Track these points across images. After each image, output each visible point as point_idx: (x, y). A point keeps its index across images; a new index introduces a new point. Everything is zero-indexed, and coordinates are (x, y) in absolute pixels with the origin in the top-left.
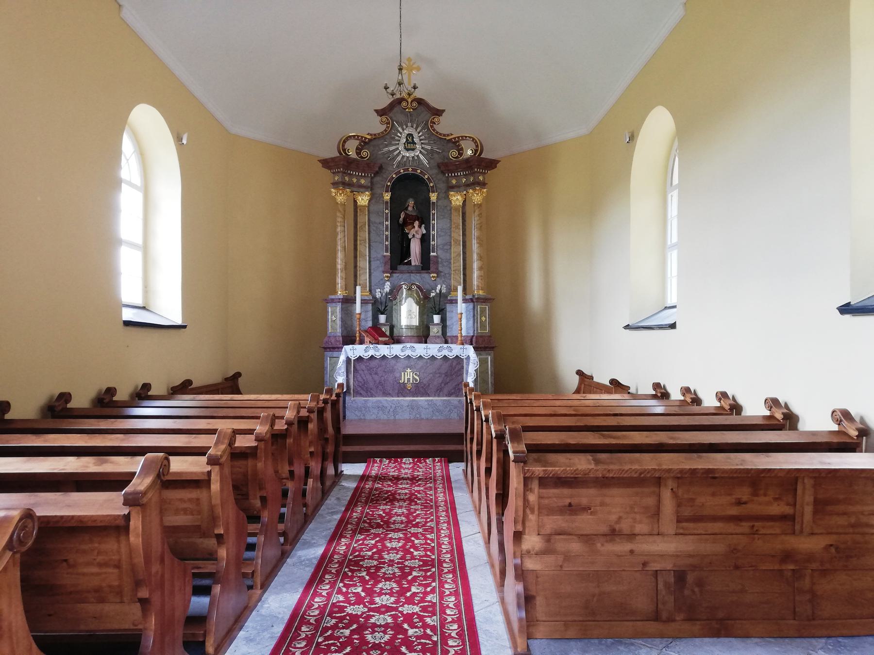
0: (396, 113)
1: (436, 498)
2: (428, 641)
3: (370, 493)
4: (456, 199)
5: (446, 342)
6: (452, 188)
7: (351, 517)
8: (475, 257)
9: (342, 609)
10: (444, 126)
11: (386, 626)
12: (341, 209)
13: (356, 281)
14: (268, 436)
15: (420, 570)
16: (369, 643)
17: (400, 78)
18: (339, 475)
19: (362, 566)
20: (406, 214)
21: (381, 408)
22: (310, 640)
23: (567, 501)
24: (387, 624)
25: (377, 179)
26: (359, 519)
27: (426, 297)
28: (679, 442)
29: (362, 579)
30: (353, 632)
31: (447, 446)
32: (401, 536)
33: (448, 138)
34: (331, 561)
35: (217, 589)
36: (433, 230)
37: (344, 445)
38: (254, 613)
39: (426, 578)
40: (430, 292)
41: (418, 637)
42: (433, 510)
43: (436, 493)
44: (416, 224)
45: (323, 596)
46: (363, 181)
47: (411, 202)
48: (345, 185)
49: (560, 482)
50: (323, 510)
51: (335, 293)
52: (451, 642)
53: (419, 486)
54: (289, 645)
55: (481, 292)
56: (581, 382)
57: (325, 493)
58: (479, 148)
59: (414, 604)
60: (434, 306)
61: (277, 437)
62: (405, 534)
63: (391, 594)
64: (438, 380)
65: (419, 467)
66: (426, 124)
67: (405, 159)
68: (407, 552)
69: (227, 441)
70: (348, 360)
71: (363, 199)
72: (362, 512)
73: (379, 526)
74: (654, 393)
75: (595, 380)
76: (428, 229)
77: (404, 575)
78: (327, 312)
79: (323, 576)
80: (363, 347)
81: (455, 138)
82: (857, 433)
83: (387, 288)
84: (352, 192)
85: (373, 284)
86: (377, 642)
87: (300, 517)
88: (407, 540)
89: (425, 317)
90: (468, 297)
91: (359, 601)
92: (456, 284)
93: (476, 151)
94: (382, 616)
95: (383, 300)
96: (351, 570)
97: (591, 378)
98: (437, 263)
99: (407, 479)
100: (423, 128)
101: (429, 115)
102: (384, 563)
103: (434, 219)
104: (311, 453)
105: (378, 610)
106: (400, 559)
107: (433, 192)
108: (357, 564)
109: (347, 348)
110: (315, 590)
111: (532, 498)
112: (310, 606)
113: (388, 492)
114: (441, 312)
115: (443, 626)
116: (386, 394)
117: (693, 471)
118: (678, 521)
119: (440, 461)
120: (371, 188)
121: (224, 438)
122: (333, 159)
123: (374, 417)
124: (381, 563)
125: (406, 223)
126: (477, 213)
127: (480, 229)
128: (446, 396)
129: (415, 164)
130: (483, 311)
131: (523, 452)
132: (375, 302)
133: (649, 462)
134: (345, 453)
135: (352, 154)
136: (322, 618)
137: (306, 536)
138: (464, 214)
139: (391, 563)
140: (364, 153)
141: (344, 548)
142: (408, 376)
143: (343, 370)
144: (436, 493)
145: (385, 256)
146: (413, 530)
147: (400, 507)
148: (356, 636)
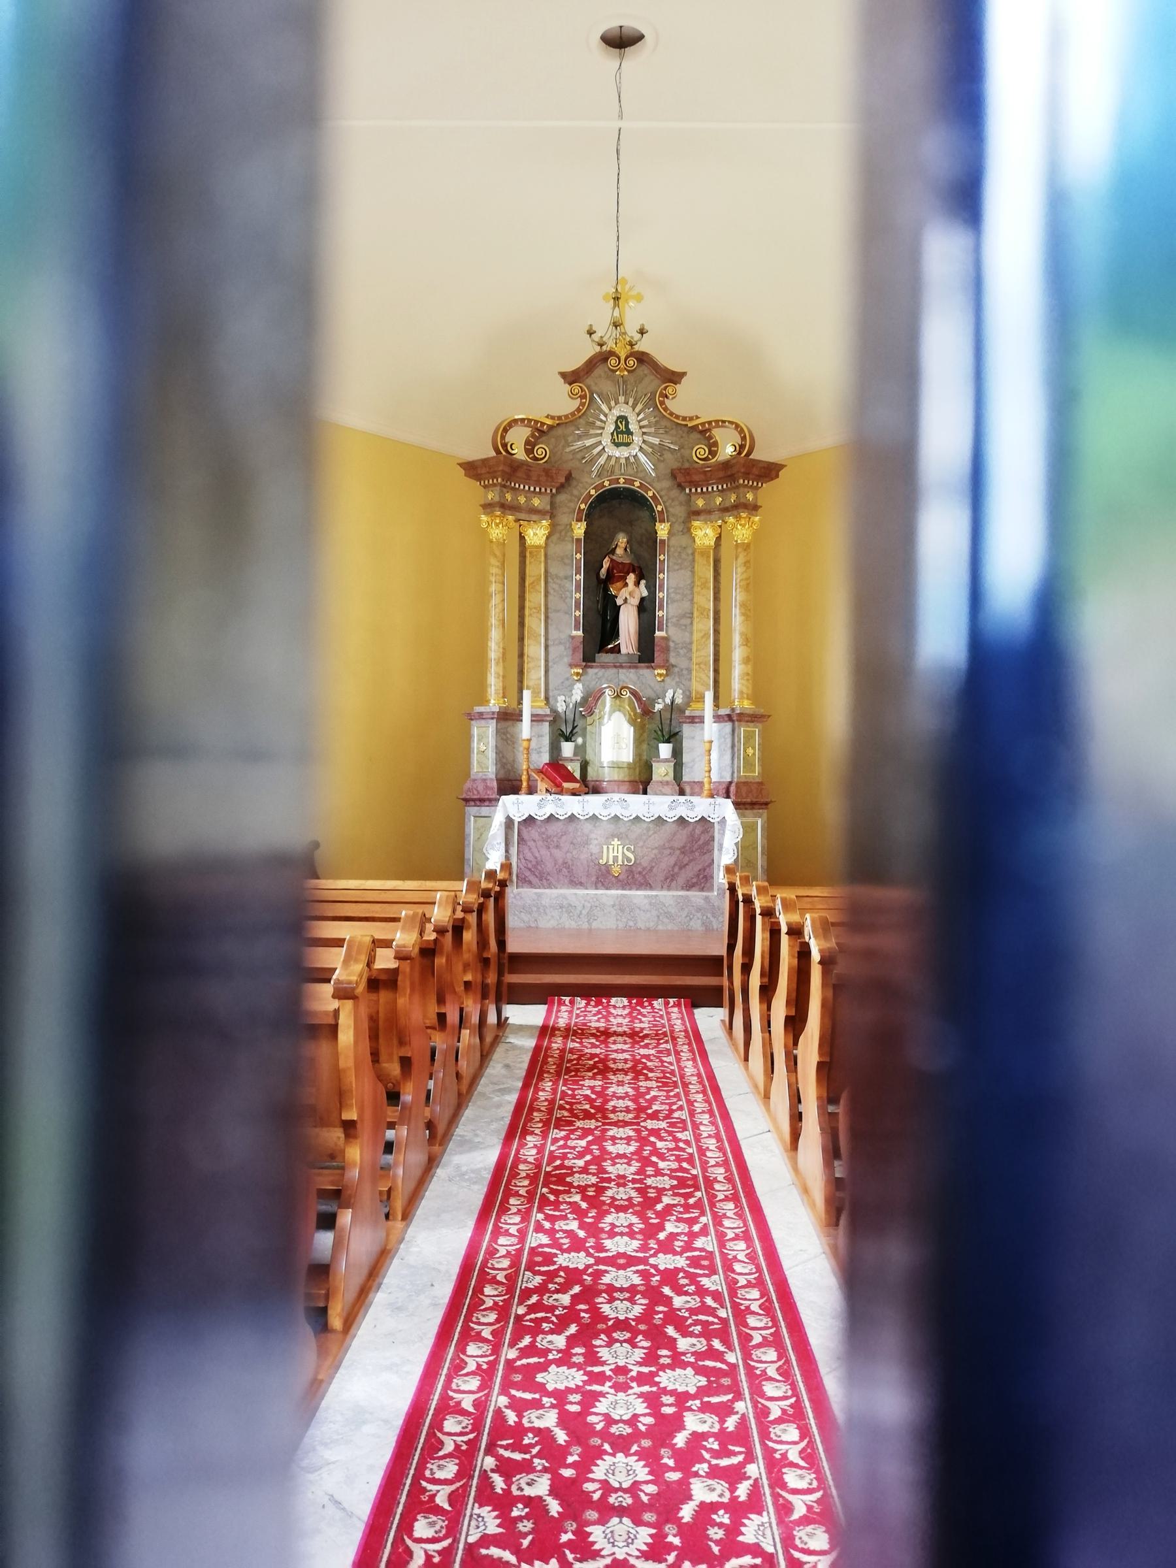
0: (600, 381)
1: (681, 1069)
2: (711, 1319)
3: (562, 1057)
4: (704, 534)
5: (682, 793)
6: (697, 513)
7: (535, 1099)
8: (737, 639)
9: (549, 1259)
10: (685, 402)
11: (632, 1290)
12: (498, 553)
13: (521, 681)
14: (417, 950)
15: (675, 1195)
16: (606, 1319)
17: (616, 313)
18: (502, 1023)
19: (570, 1185)
20: (612, 560)
21: (565, 908)
22: (503, 1311)
24: (633, 1286)
25: (562, 498)
26: (552, 1102)
27: (647, 711)
29: (575, 1207)
30: (576, 1299)
31: (693, 980)
32: (632, 1133)
33: (690, 424)
34: (514, 1174)
35: (345, 1218)
36: (661, 590)
37: (513, 973)
38: (396, 1262)
39: (687, 1208)
40: (653, 701)
41: (693, 1312)
42: (680, 1090)
43: (678, 1060)
44: (631, 578)
45: (485, 1340)
46: (536, 502)
47: (622, 540)
48: (505, 507)
50: (483, 1085)
51: (484, 701)
52: (752, 1321)
53: (646, 1046)
54: (468, 1318)
57: (485, 1056)
58: (746, 444)
59: (675, 1253)
60: (661, 727)
61: (428, 952)
62: (638, 1131)
63: (631, 1235)
64: (668, 862)
65: (640, 1013)
66: (652, 398)
67: (613, 462)
68: (646, 1162)
69: (364, 958)
70: (509, 823)
71: (537, 534)
72: (554, 1091)
73: (587, 1116)
76: (651, 588)
77: (649, 1203)
78: (469, 737)
79: (505, 1200)
80: (535, 798)
81: (703, 424)
83: (577, 694)
84: (517, 520)
85: (551, 687)
86: (622, 1317)
87: (452, 1098)
88: (643, 1141)
89: (645, 746)
90: (723, 711)
91: (577, 1245)
92: (700, 688)
93: (742, 447)
94: (621, 1272)
95: (570, 716)
96: (552, 1192)
98: (666, 650)
99: (624, 1034)
100: (646, 406)
101: (657, 382)
102: (609, 1180)
103: (662, 571)
104: (466, 982)
105: (612, 1261)
106: (636, 1173)
107: (662, 521)
108: (561, 1180)
109: (507, 800)
110: (496, 1226)
112: (491, 1253)
113: (593, 1056)
114: (673, 737)
115: (733, 1292)
116: (575, 883)
119: (678, 1005)
120: (551, 513)
121: (359, 952)
122: (484, 462)
123: (552, 923)
124: (603, 1180)
125: (611, 577)
126: (741, 559)
127: (747, 588)
128: (683, 889)
129: (630, 471)
130: (749, 737)
132: (555, 719)
134: (511, 986)
135: (519, 453)
136: (517, 1273)
137: (462, 1130)
138: (717, 562)
139: (621, 1181)
140: (539, 451)
141: (534, 1151)
142: (615, 853)
143: (501, 839)
144: (678, 1060)
145: (573, 638)
146: (651, 1124)
147: (620, 1083)
148: (582, 1307)
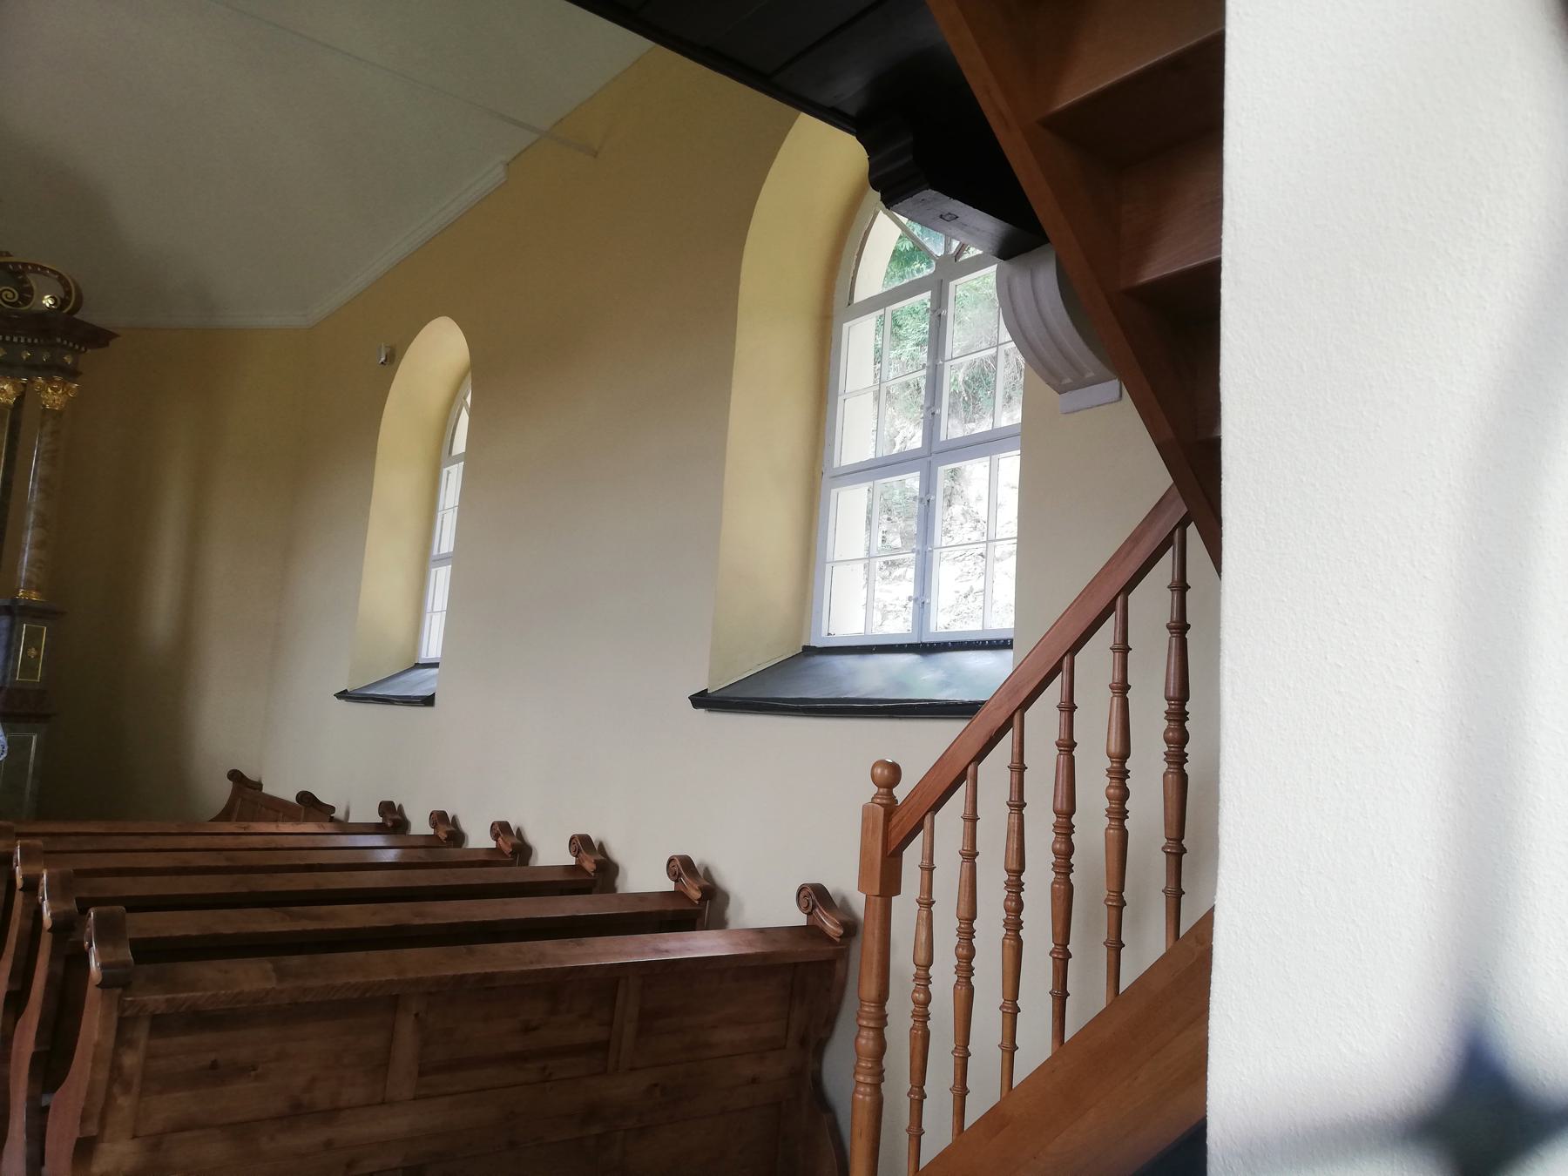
23: (213, 1056)
28: (431, 921)
49: (199, 1019)
55: (34, 596)
56: (236, 793)
58: (70, 297)
74: (380, 820)
75: (265, 790)
82: (699, 895)
97: (258, 786)
111: (130, 1060)
117: (461, 980)
118: (421, 1074)
131: (125, 965)
133: (379, 967)
